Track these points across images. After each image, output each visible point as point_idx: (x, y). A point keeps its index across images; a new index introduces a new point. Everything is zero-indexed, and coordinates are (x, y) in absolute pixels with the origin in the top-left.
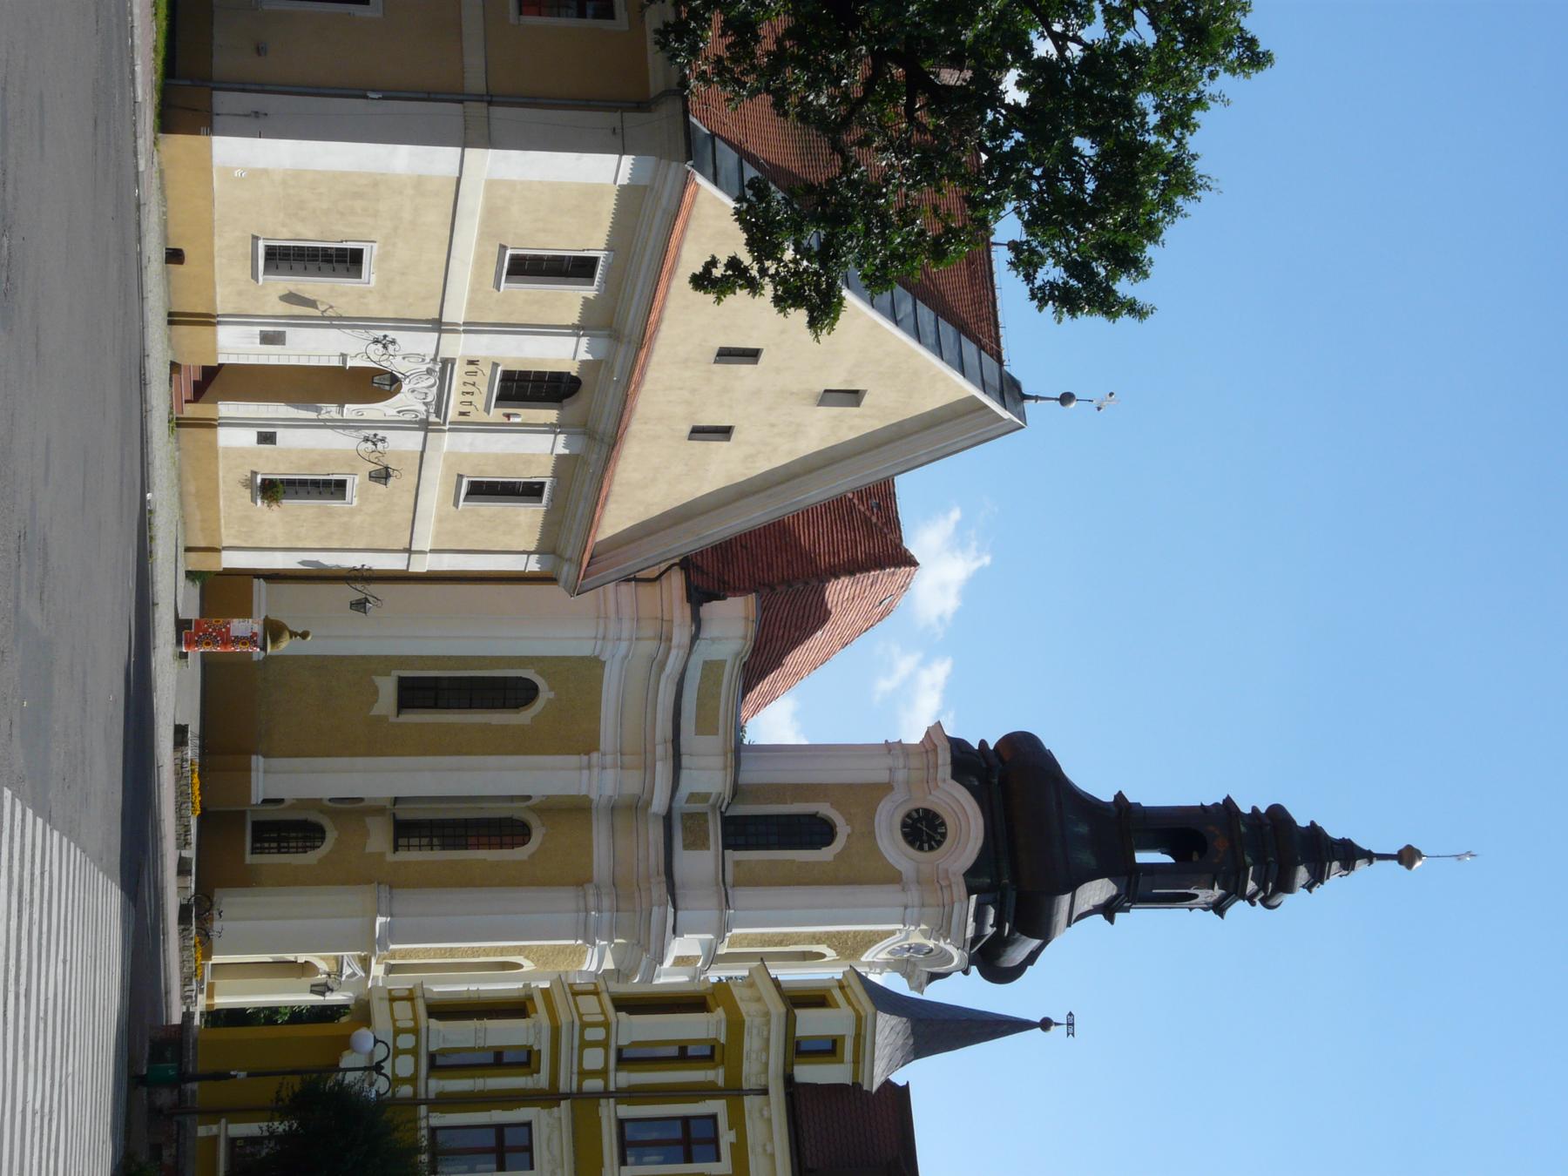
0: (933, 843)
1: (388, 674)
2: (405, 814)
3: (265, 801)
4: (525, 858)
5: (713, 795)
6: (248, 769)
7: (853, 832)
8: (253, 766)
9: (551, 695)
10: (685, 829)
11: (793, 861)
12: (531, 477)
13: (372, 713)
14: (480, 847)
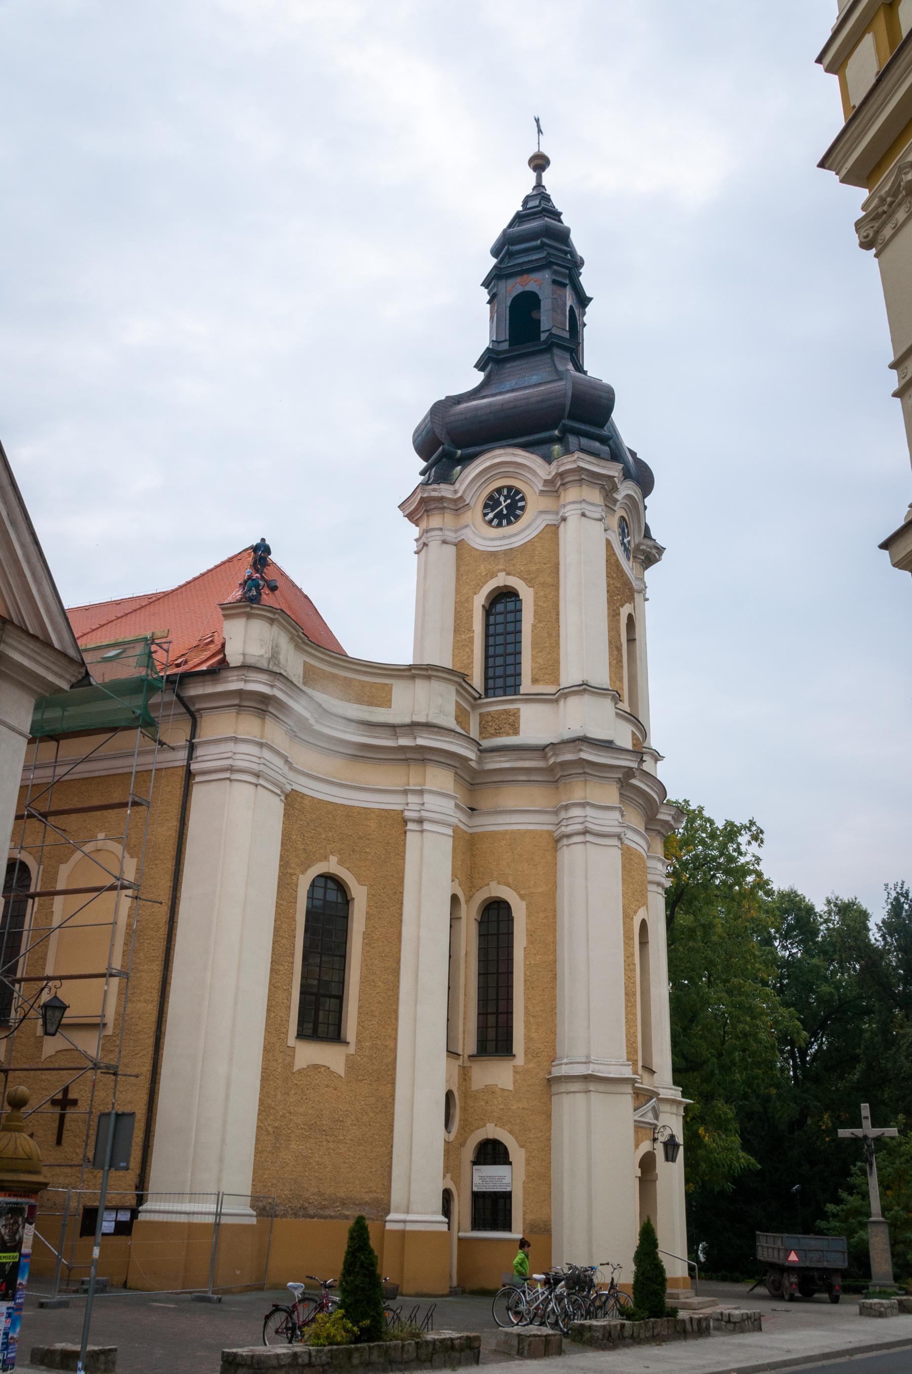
0: (517, 498)
1: (293, 1049)
2: (469, 1043)
3: (447, 1211)
4: (524, 904)
5: (459, 700)
6: (403, 1233)
7: (504, 570)
8: (399, 1227)
9: (333, 859)
10: (497, 734)
11: (534, 626)
14: (510, 997)
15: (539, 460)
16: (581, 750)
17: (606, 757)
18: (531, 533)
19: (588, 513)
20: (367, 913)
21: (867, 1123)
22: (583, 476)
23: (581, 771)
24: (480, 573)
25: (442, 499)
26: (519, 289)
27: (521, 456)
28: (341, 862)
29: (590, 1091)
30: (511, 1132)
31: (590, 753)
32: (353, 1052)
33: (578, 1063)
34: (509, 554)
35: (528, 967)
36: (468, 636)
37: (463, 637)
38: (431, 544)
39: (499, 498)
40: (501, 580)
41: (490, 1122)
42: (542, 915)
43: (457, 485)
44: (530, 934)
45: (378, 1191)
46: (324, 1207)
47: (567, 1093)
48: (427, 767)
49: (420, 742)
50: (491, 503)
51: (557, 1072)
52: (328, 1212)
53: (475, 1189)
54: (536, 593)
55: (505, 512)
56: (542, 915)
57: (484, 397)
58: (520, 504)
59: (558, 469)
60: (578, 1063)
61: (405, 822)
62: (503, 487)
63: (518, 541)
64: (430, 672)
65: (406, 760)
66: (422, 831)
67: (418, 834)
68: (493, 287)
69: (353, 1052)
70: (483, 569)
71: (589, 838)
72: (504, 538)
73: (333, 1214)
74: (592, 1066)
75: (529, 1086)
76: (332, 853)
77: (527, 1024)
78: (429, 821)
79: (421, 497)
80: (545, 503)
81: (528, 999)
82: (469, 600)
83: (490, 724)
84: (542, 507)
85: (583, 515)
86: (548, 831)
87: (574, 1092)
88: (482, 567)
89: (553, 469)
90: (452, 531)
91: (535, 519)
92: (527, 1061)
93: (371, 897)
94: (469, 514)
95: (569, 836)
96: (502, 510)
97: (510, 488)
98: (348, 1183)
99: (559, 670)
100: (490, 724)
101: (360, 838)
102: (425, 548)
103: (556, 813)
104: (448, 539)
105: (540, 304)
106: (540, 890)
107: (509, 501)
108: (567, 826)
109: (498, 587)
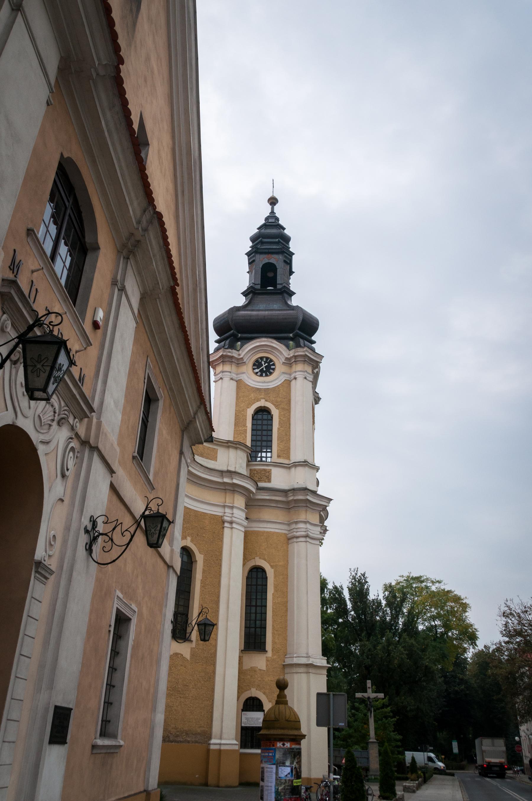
0: (271, 364)
4: (273, 570)
8: (217, 747)
11: (278, 429)
12: (144, 382)
13: (189, 659)
15: (284, 347)
16: (307, 495)
17: (317, 499)
18: (278, 383)
19: (307, 378)
20: (203, 569)
21: (369, 691)
22: (306, 359)
23: (305, 505)
24: (251, 398)
25: (232, 357)
26: (266, 261)
27: (275, 344)
28: (192, 541)
29: (310, 672)
30: (264, 693)
31: (311, 497)
32: (194, 647)
33: (303, 657)
34: (267, 391)
35: (274, 604)
36: (243, 428)
37: (241, 428)
38: (224, 379)
39: (261, 362)
40: (262, 403)
41: (253, 688)
42: (281, 577)
43: (240, 352)
44: (276, 587)
45: (205, 726)
46: (177, 736)
47: (296, 673)
48: (235, 495)
49: (235, 481)
50: (257, 364)
51: (288, 661)
52: (179, 739)
53: (243, 725)
54: (280, 413)
55: (264, 369)
56: (281, 577)
57: (247, 310)
58: (272, 367)
59: (294, 353)
60: (303, 657)
61: (224, 522)
62: (264, 357)
63: (272, 385)
64: (238, 446)
65: (225, 490)
66: (232, 528)
67: (230, 529)
68: (253, 256)
69: (194, 647)
70: (252, 395)
71: (308, 539)
72: (265, 382)
73: (182, 740)
74: (311, 659)
75: (274, 668)
76: (188, 535)
77: (273, 634)
78: (235, 523)
79: (222, 354)
80: (284, 369)
81: (274, 621)
82: (245, 411)
83: (256, 475)
84: (283, 370)
85: (305, 378)
86: (284, 533)
87: (300, 673)
88: (252, 395)
89: (292, 353)
90: (235, 374)
91: (279, 377)
92: (273, 654)
93: (205, 561)
94: (245, 367)
95: (297, 537)
96: (263, 368)
97: (267, 358)
98: (190, 722)
99: (290, 452)
100: (256, 475)
101: (201, 528)
102: (221, 380)
103: (289, 525)
104: (234, 378)
105: (277, 270)
106: (280, 564)
107: (267, 364)
108: (297, 532)
109: (261, 407)
